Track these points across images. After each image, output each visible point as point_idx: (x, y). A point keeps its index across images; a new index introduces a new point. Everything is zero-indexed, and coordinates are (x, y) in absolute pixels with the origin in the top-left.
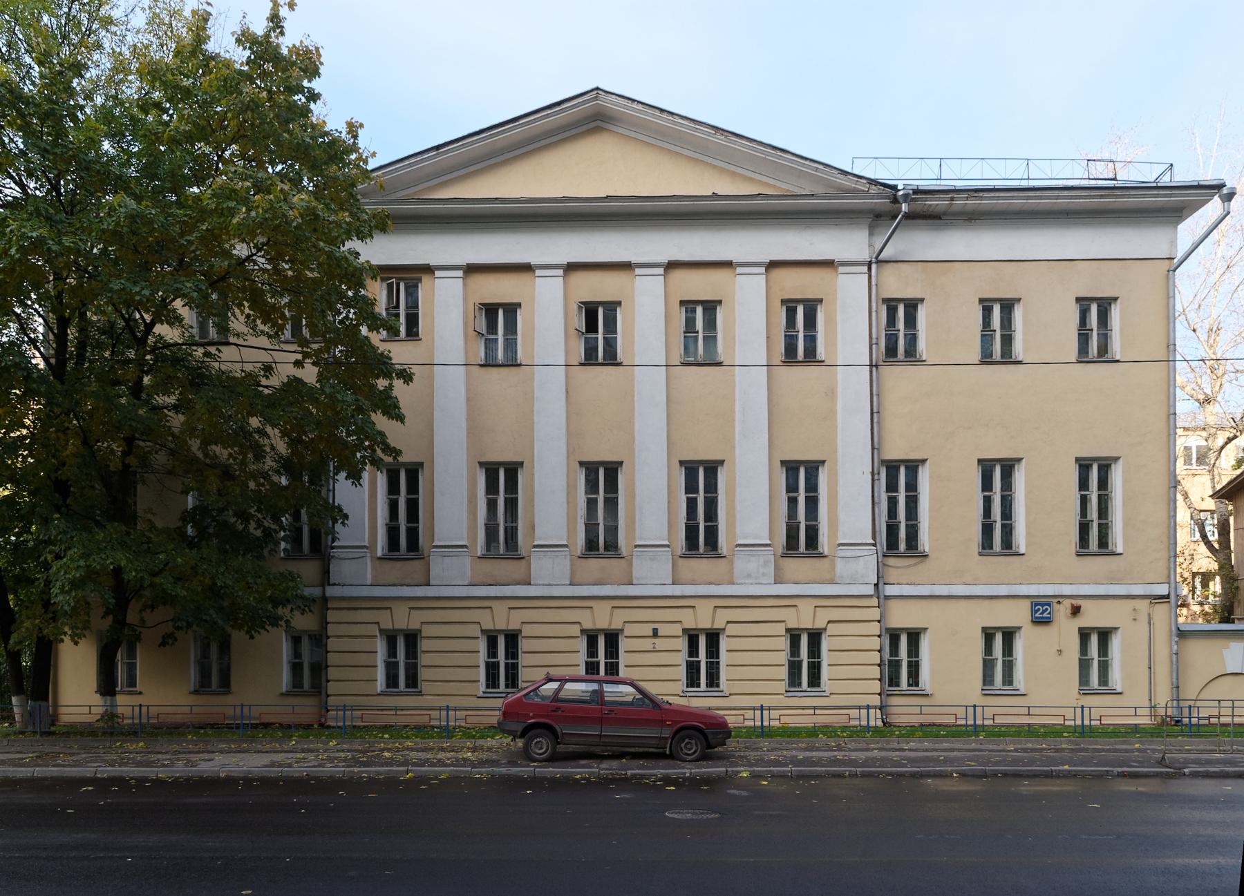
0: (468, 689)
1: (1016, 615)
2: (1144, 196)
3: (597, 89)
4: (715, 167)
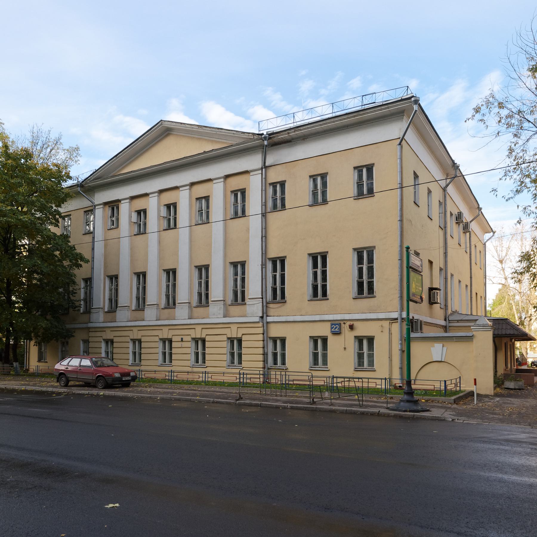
0: (125, 362)
1: (324, 330)
2: (375, 111)
4: (206, 140)
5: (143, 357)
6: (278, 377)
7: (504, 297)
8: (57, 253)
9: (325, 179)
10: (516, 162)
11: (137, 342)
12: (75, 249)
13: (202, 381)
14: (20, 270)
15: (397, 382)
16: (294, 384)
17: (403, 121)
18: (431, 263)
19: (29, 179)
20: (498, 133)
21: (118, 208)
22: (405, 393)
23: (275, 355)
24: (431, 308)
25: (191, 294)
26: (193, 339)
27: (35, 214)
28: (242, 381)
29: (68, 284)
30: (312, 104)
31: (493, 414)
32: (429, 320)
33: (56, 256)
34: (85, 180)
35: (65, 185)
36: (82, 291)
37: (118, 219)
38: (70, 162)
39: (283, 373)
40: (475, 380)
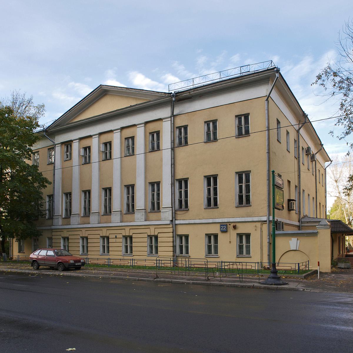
0: (77, 253)
1: (216, 229)
2: (249, 77)
3: (101, 85)
4: (132, 97)
5: (89, 249)
6: (184, 262)
7: (338, 206)
8: (30, 178)
9: (215, 123)
10: (346, 113)
11: (85, 239)
12: (42, 175)
13: (131, 266)
14: (5, 190)
15: (266, 265)
16: (195, 267)
17: (268, 84)
18: (289, 182)
19: (11, 127)
20: (334, 93)
21: (71, 146)
22: (272, 272)
23: (181, 247)
24: (289, 213)
25: (122, 205)
26: (124, 236)
27: (15, 151)
28: (158, 265)
29: (38, 199)
30: (206, 72)
31: (330, 285)
32: (288, 222)
33: (29, 180)
34: (49, 127)
35: (35, 131)
36: (47, 203)
37: (71, 154)
38: (38, 115)
39: (187, 260)
40: (319, 262)
